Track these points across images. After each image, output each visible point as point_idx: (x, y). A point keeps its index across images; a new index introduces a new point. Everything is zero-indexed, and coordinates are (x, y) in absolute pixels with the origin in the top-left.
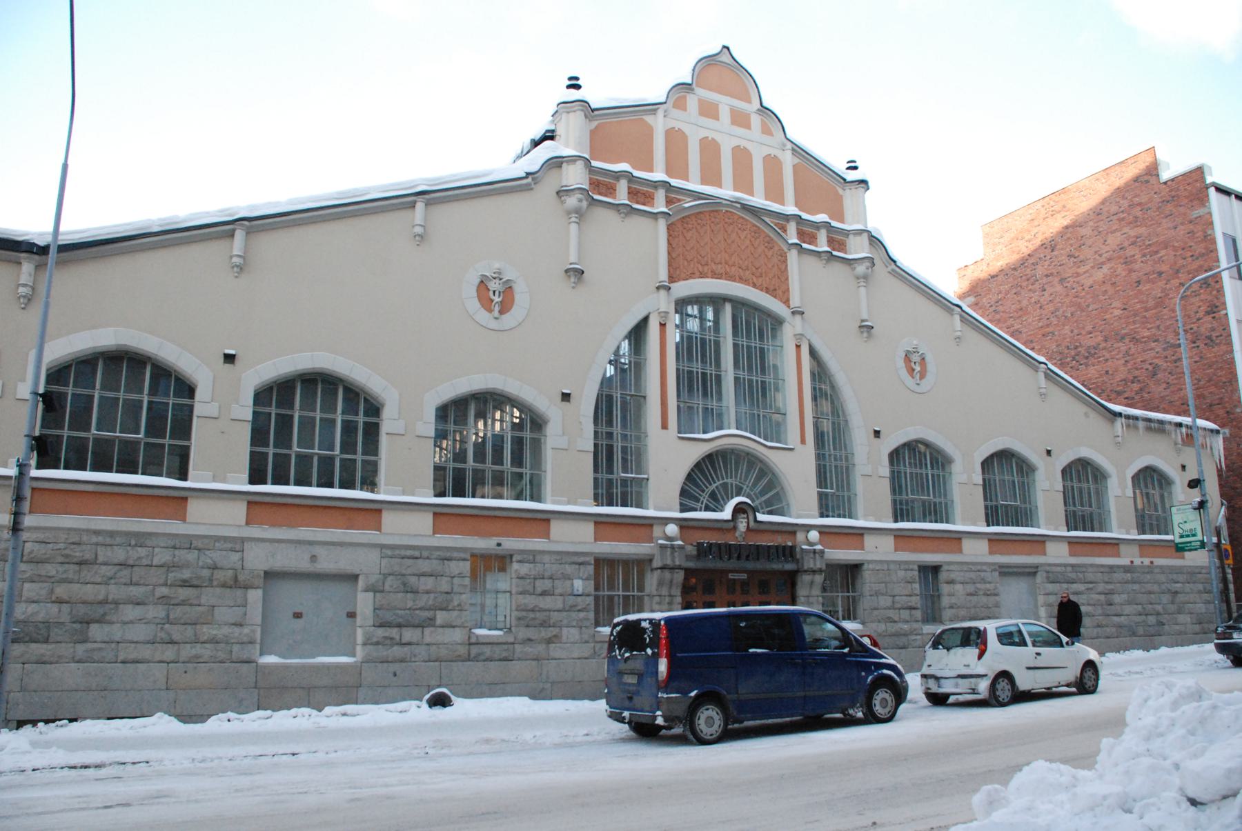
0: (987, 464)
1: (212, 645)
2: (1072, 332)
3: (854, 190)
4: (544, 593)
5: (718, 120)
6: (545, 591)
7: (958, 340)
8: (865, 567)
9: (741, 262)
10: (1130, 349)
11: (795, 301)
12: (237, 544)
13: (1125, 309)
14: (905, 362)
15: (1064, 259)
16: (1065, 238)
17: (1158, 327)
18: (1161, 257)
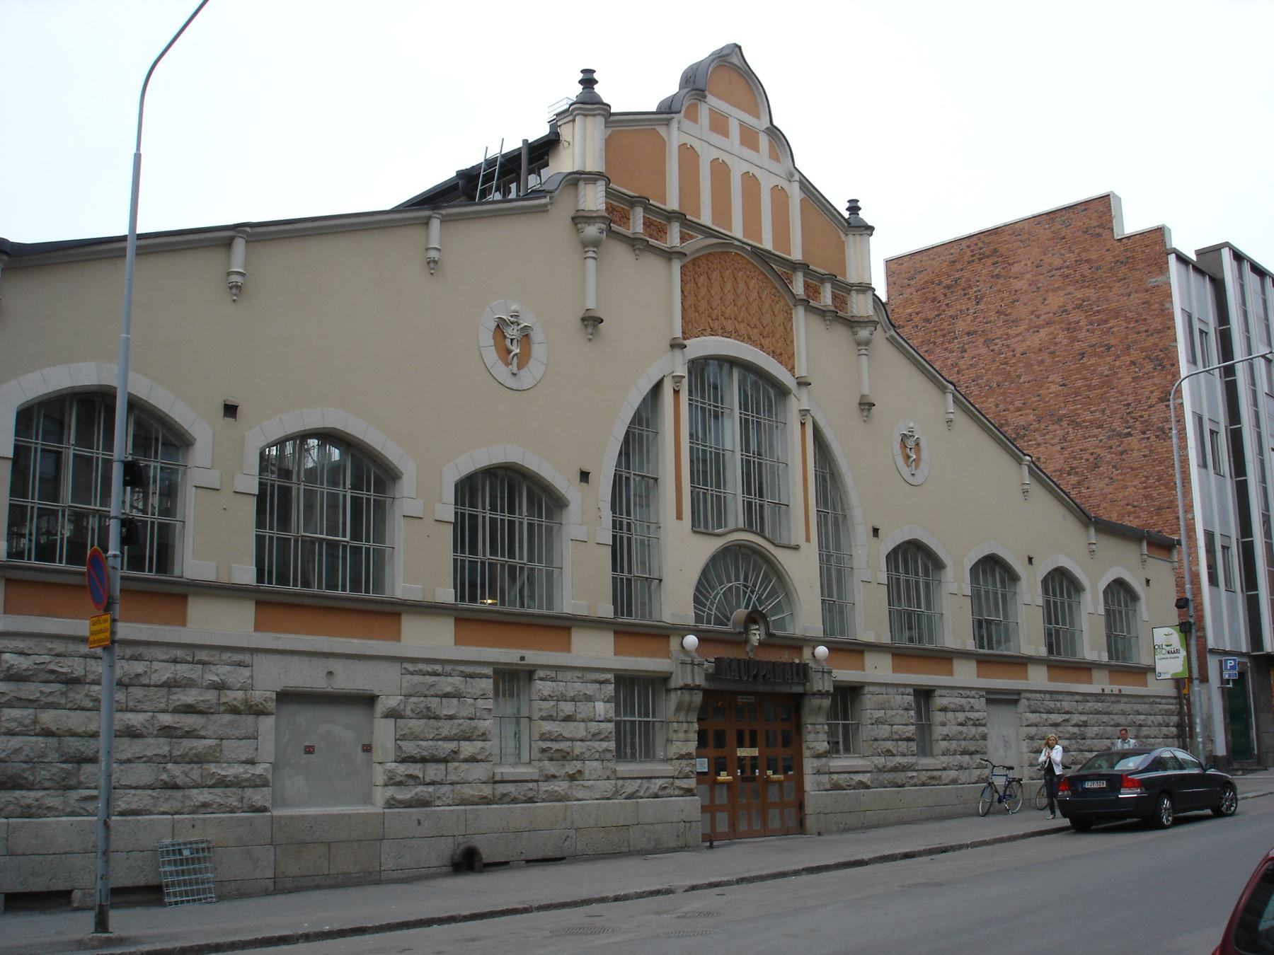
0: (468, 488)
1: (221, 790)
2: (997, 406)
3: (858, 237)
4: (568, 719)
5: (728, 138)
6: (569, 716)
7: (432, 265)
8: (867, 689)
9: (750, 319)
10: (1068, 433)
11: (801, 370)
12: (242, 654)
13: (1063, 385)
14: (901, 447)
15: (992, 316)
16: (995, 289)
17: (1103, 411)
18: (1111, 328)
